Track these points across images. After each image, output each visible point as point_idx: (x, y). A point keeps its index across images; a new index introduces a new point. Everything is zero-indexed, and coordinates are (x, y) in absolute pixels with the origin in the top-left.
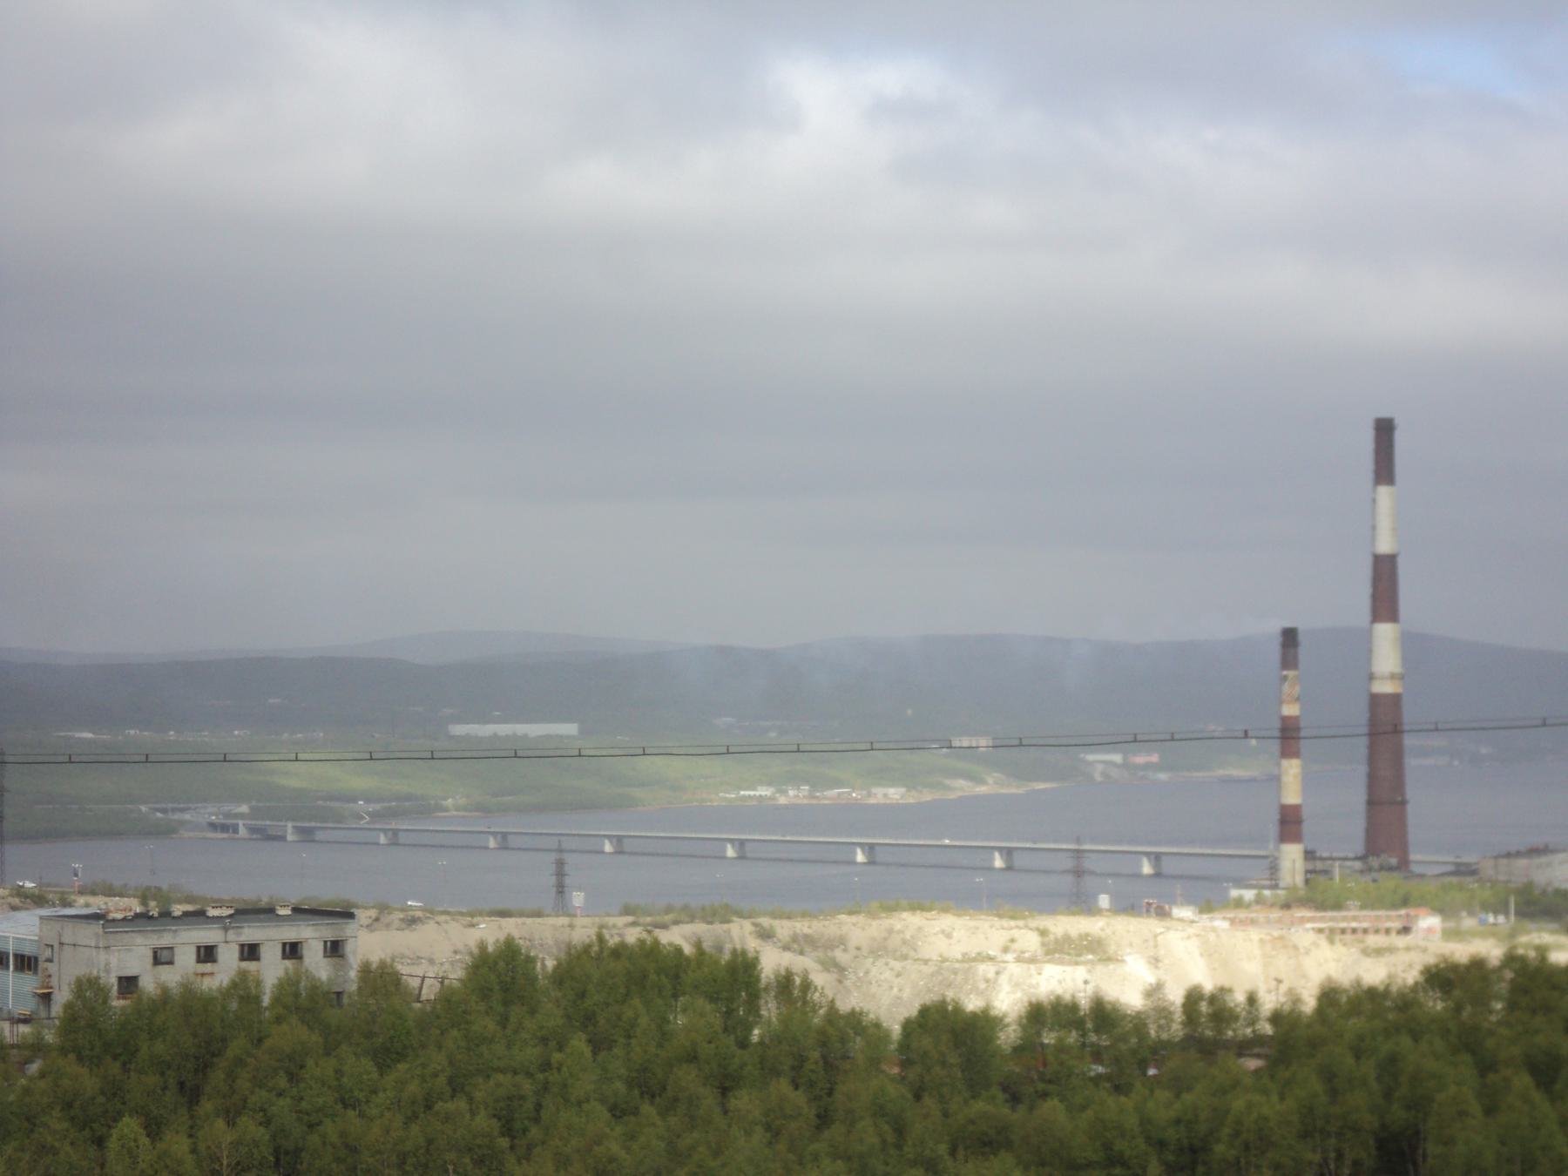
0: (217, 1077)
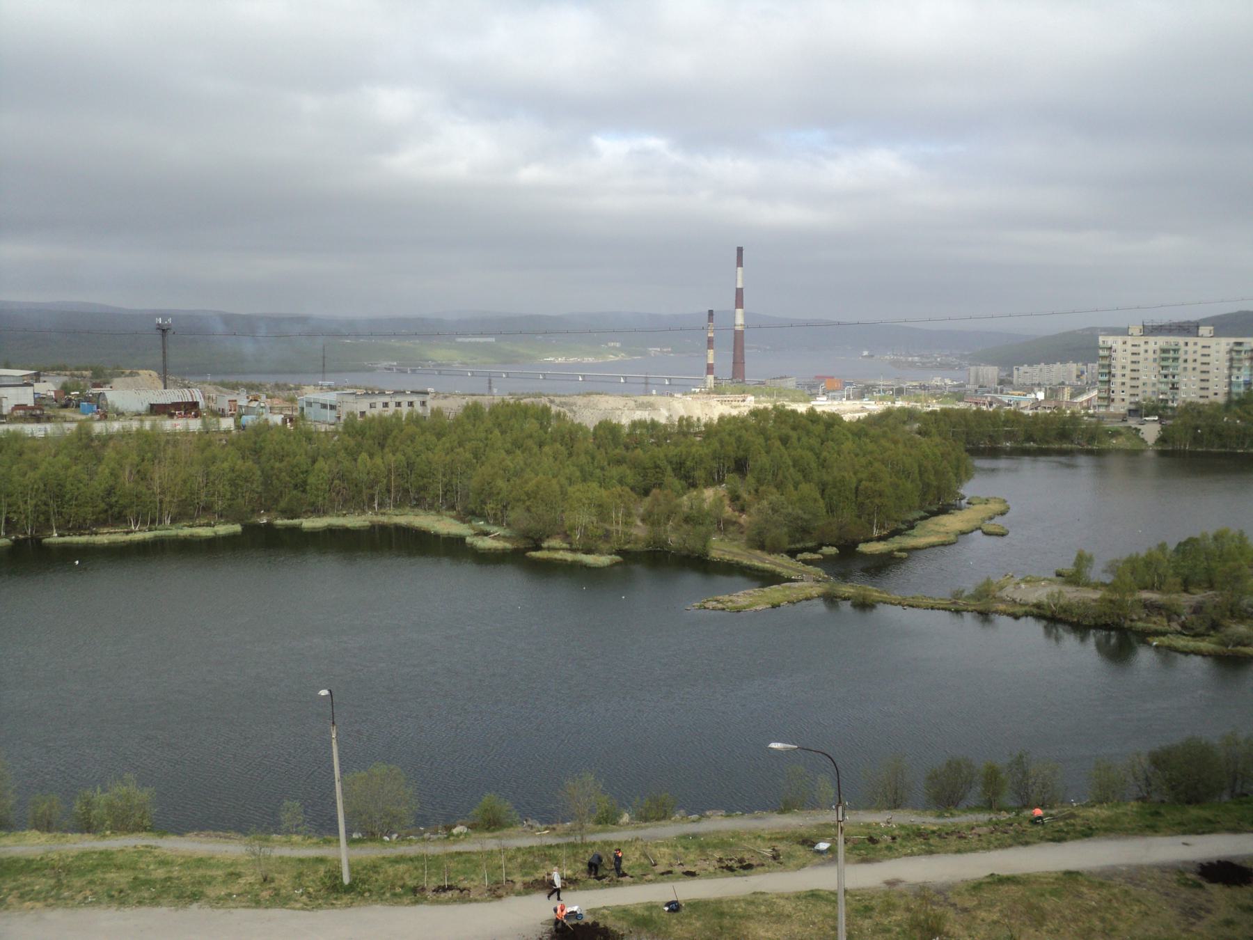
0: (390, 441)
